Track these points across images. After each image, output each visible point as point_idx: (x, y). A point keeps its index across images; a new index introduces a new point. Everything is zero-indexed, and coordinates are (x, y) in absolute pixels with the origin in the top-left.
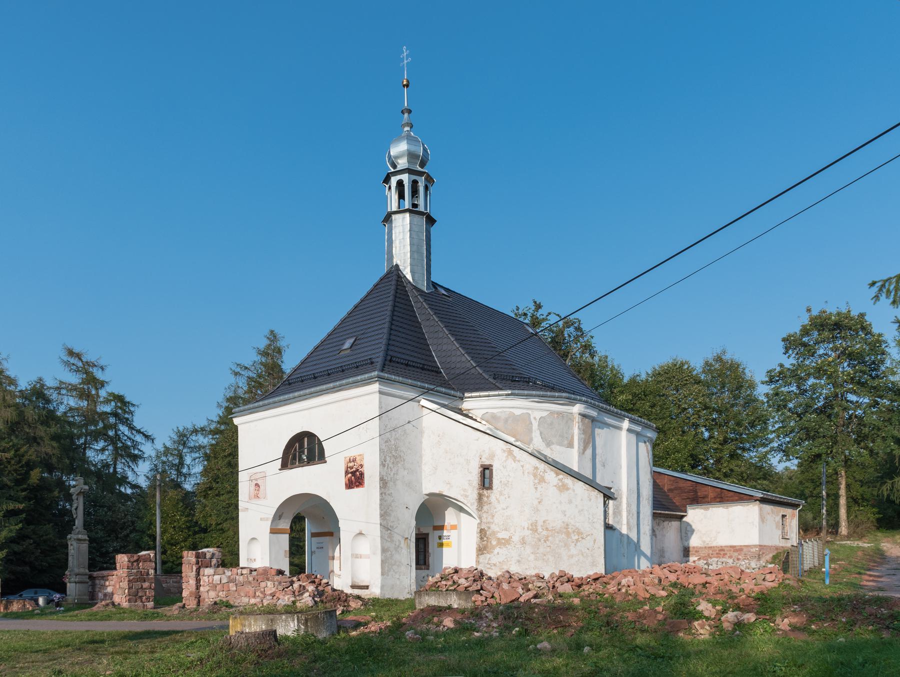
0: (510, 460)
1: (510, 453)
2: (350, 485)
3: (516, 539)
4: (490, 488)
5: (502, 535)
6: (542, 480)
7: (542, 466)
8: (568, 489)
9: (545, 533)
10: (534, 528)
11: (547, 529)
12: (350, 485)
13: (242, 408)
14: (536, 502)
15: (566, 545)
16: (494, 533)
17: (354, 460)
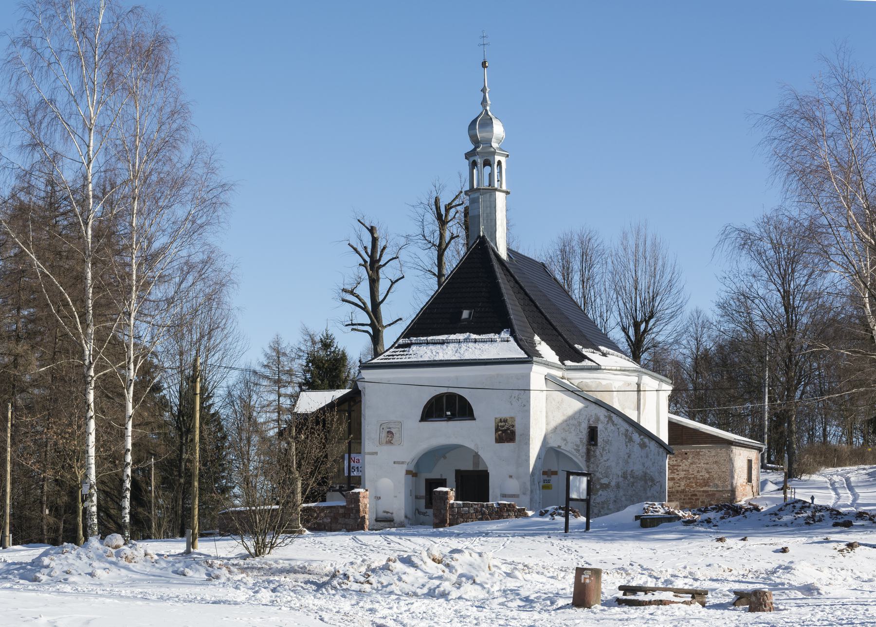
0: (610, 424)
1: (610, 418)
2: (499, 440)
3: (613, 484)
4: (596, 444)
5: (604, 481)
6: (631, 440)
7: (631, 429)
8: (646, 446)
9: (632, 480)
10: (625, 476)
11: (633, 477)
12: (499, 440)
13: (754, 473)
14: (626, 457)
15: (645, 490)
16: (599, 479)
17: (505, 421)
